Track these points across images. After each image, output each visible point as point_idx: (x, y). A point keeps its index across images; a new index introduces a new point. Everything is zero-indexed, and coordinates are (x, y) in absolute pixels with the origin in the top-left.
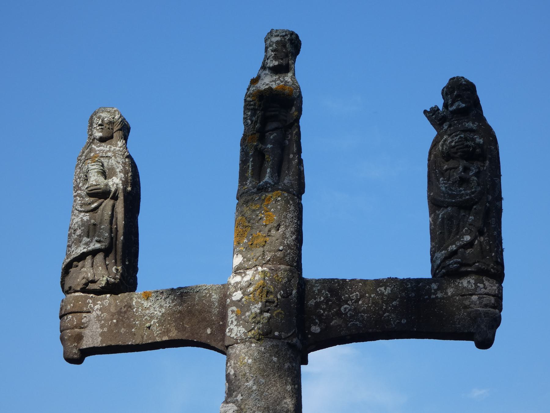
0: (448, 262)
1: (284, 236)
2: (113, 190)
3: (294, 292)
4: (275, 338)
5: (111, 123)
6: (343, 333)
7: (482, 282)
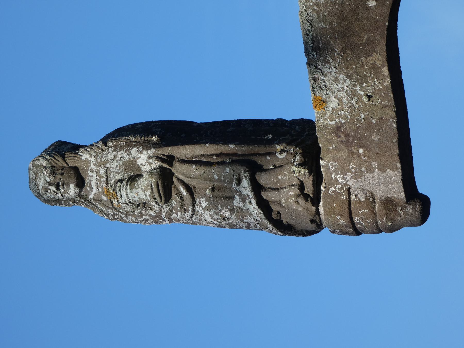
2: (157, 164)
5: (53, 171)
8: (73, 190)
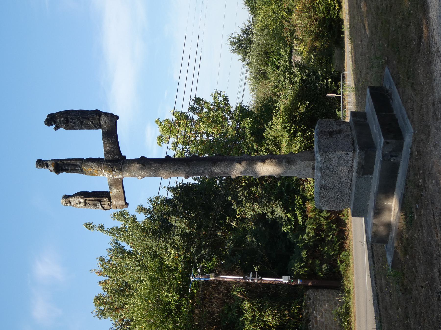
0: (97, 127)
1: (95, 166)
2: (84, 201)
3: (109, 164)
4: (121, 168)
5: (66, 202)
6: (118, 151)
7: (102, 119)
8: (69, 204)
